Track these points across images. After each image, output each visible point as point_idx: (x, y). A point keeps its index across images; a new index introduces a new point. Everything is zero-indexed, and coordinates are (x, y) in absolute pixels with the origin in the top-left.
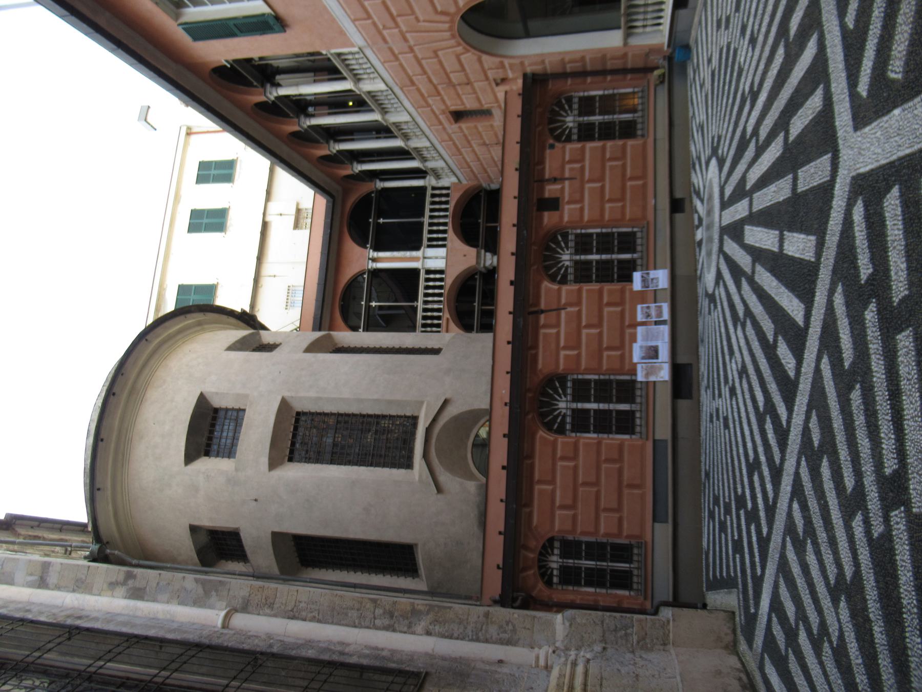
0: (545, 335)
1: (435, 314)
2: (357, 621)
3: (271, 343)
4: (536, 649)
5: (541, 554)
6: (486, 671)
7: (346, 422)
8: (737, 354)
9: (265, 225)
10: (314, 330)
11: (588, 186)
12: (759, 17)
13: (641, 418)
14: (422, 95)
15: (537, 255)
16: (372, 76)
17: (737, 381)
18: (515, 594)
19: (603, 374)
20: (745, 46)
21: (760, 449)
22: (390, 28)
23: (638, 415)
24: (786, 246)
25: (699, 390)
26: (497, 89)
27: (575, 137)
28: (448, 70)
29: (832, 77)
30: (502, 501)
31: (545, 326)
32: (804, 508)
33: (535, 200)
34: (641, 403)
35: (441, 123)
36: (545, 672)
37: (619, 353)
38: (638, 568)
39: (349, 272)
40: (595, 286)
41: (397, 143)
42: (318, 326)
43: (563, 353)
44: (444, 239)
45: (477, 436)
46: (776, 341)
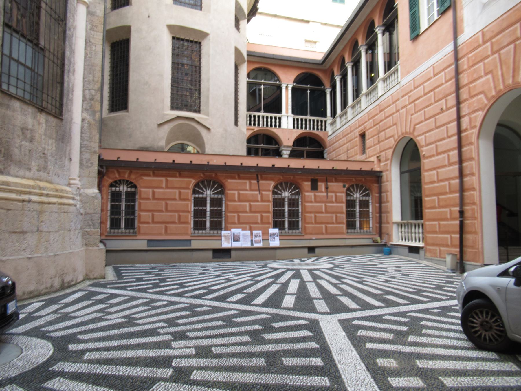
0: (246, 183)
1: (257, 123)
2: (86, 79)
3: (240, 27)
4: (79, 179)
5: (127, 181)
6: (65, 152)
7: (196, 71)
8: (237, 278)
9: (308, 22)
10: (248, 52)
11: (323, 205)
12: (397, 283)
13: (202, 233)
14: (374, 116)
15: (289, 179)
16: (386, 88)
17: (224, 278)
18: (104, 167)
19: (225, 214)
20: (385, 278)
21: (190, 288)
22: (409, 100)
23: (204, 231)
24: (289, 296)
25: (217, 262)
27: (349, 198)
28: (386, 131)
29: (364, 312)
30: (155, 160)
31: (250, 183)
32: (165, 306)
33: (317, 178)
35: (359, 126)
36: (67, 183)
38: (122, 232)
39: (280, 73)
40: (271, 209)
41: (364, 89)
42: (250, 54)
43: (236, 192)
44: (298, 128)
45: (188, 145)
46: (244, 293)
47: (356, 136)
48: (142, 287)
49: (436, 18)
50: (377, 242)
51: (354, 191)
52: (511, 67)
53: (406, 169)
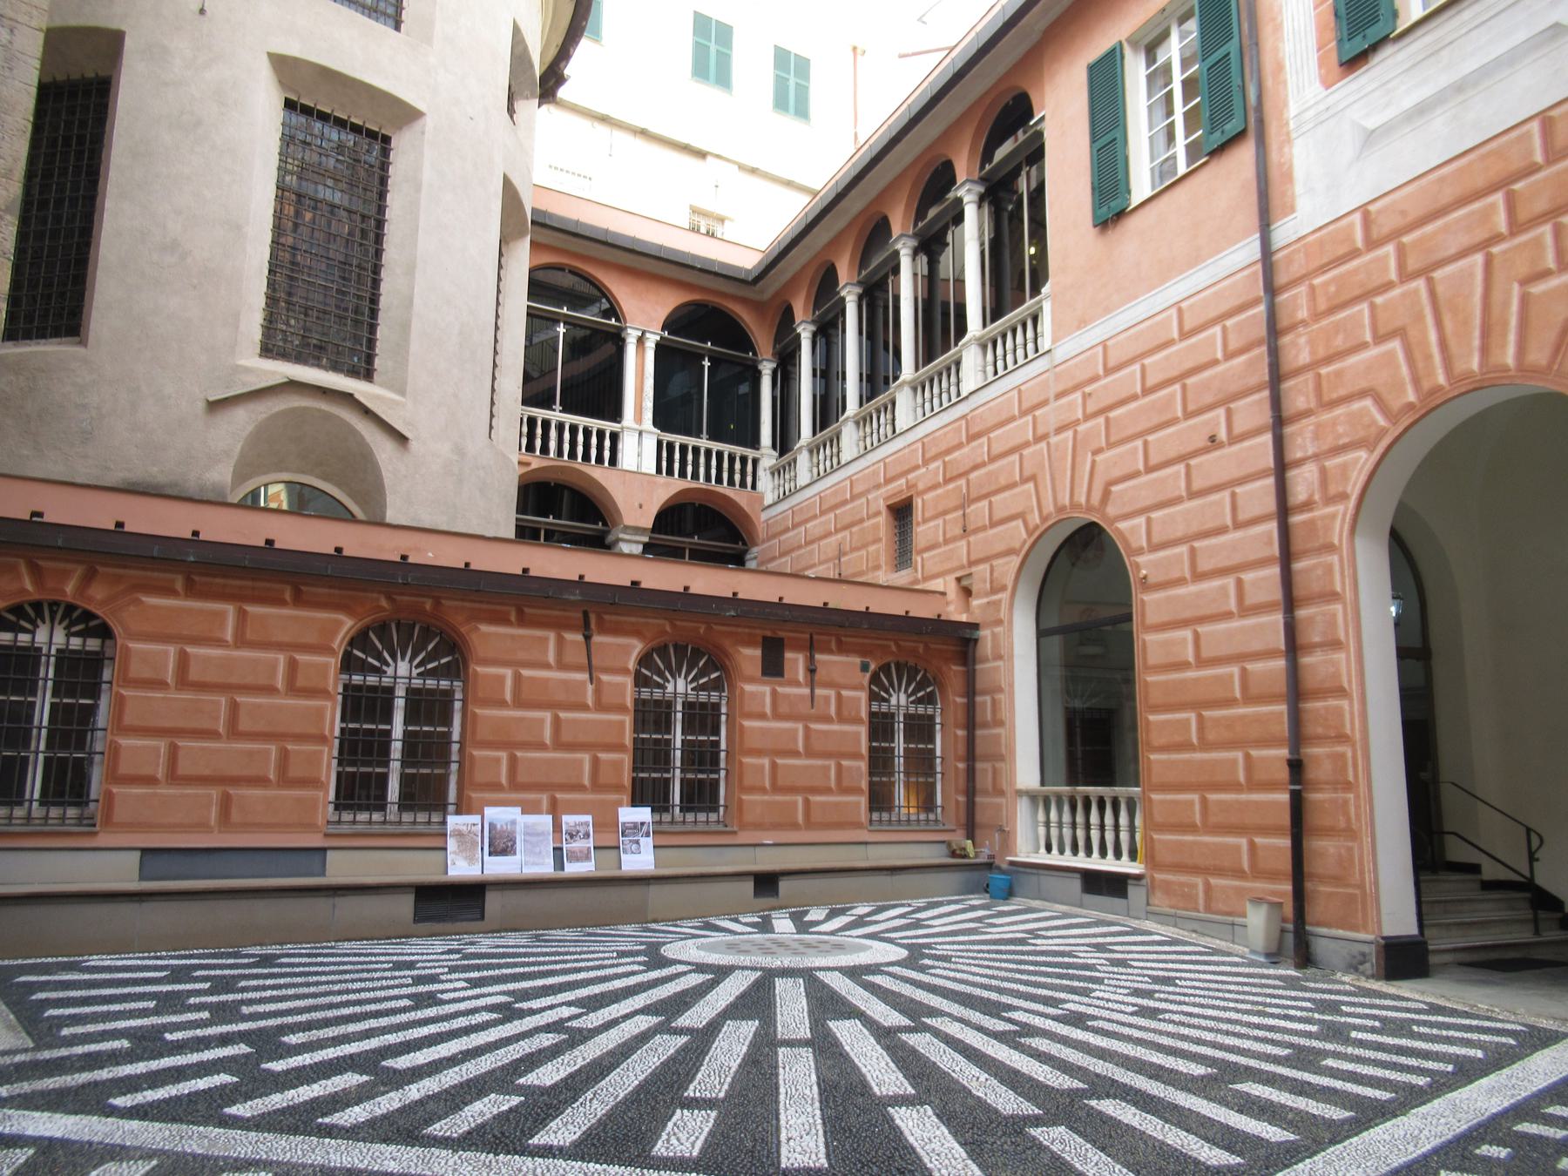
0: (547, 639)
5: (70, 608)
9: (702, 155)
13: (370, 822)
14: (949, 451)
19: (461, 750)
23: (376, 816)
26: (951, 579)
31: (560, 642)
33: (781, 634)
34: (400, 823)
35: (888, 481)
37: (504, 781)
39: (625, 294)
43: (508, 673)
44: (670, 472)
47: (873, 510)
48: (185, 1087)
49: (1182, 169)
50: (965, 856)
51: (892, 685)
52: (1477, 322)
53: (1052, 622)
